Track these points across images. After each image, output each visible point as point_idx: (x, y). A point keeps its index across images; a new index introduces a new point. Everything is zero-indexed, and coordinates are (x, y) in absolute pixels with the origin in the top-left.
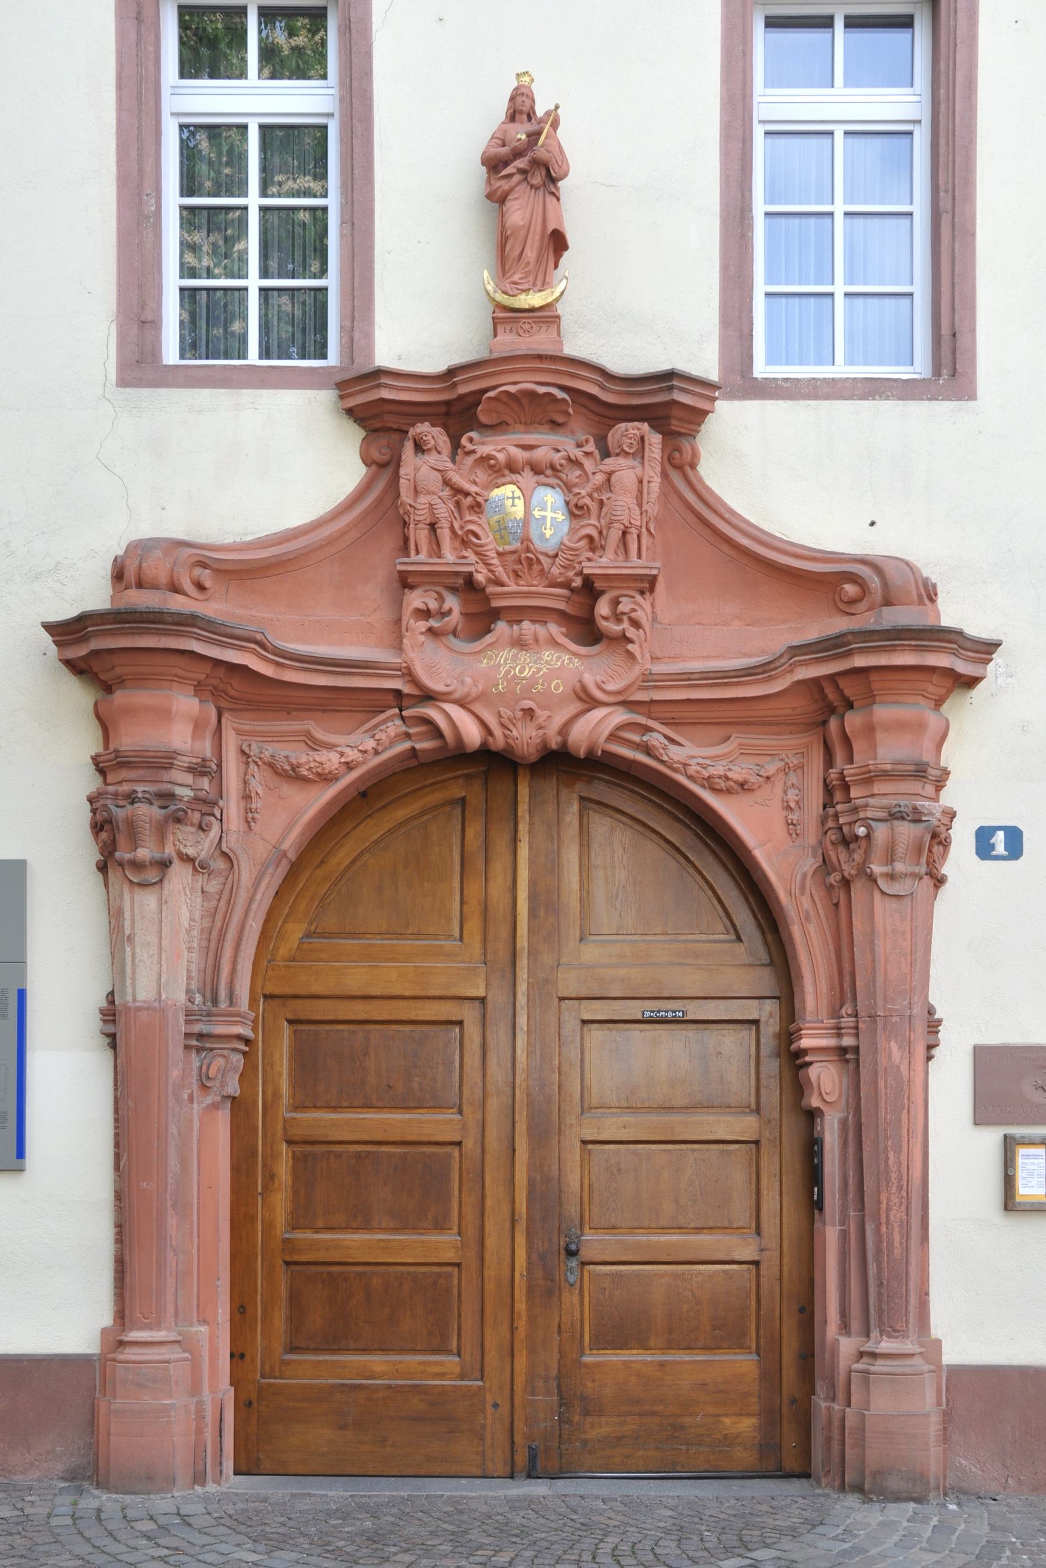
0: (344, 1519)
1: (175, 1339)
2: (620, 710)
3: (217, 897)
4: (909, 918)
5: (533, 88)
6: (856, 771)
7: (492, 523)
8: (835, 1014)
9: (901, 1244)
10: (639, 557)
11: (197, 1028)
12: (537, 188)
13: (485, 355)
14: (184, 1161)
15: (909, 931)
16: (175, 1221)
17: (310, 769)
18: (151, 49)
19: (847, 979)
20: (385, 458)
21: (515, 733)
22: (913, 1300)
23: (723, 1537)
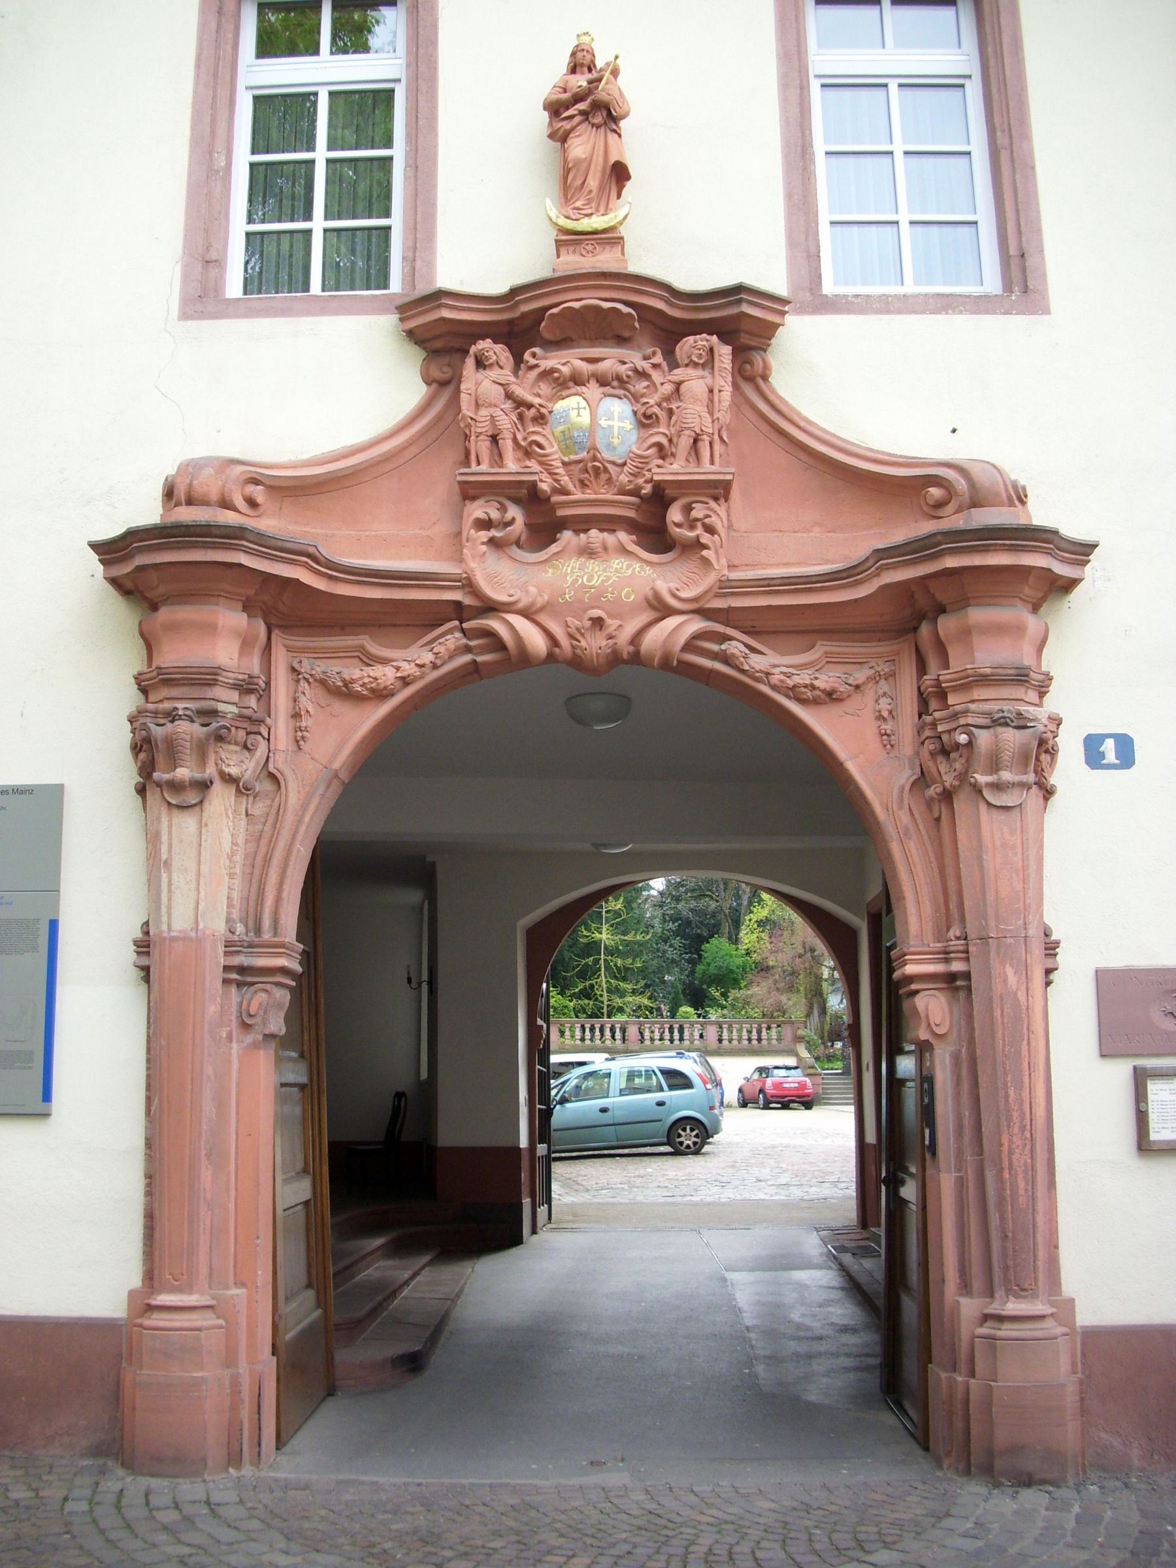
0: (395, 1513)
1: (208, 1303)
2: (696, 616)
3: (263, 820)
4: (1019, 831)
5: (593, 45)
6: (953, 676)
7: (556, 434)
8: (940, 936)
9: (1026, 1190)
10: (712, 462)
11: (237, 960)
12: (598, 127)
13: (546, 274)
14: (221, 1105)
15: (1019, 845)
16: (209, 1172)
17: (363, 685)
18: (230, 36)
19: (953, 899)
20: (447, 376)
21: (583, 643)
22: (1042, 1254)
23: (835, 1536)
